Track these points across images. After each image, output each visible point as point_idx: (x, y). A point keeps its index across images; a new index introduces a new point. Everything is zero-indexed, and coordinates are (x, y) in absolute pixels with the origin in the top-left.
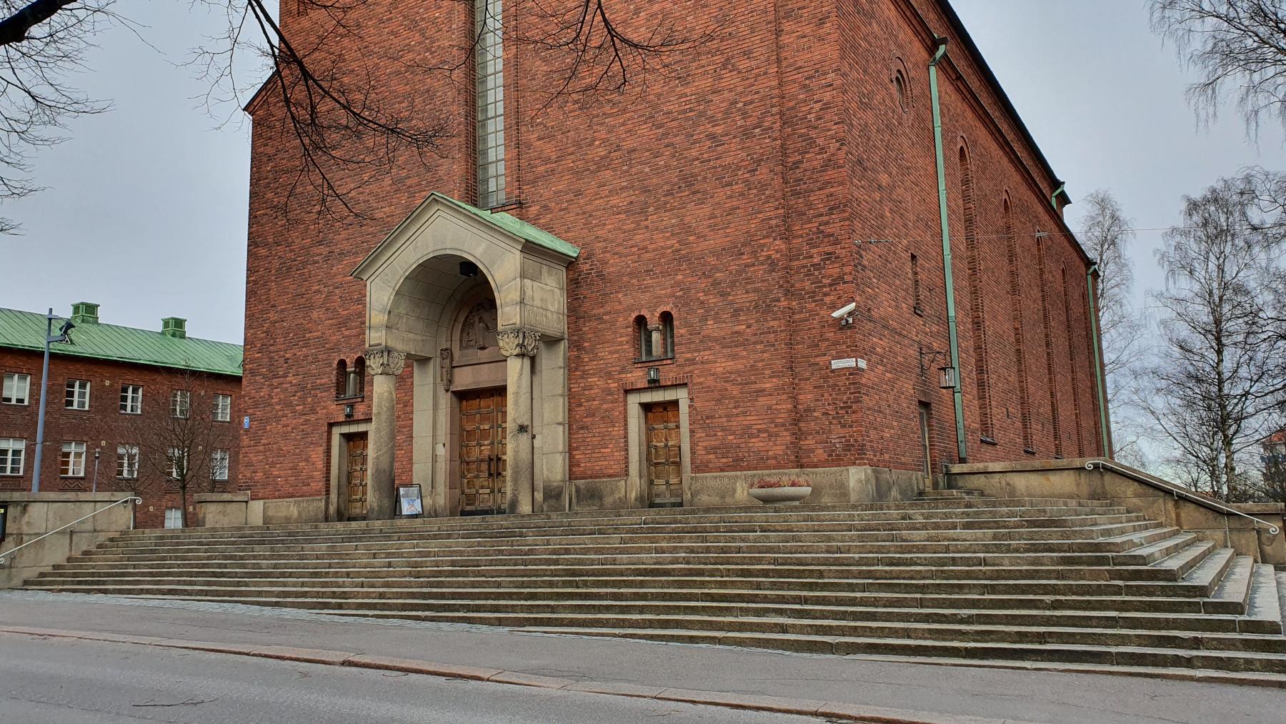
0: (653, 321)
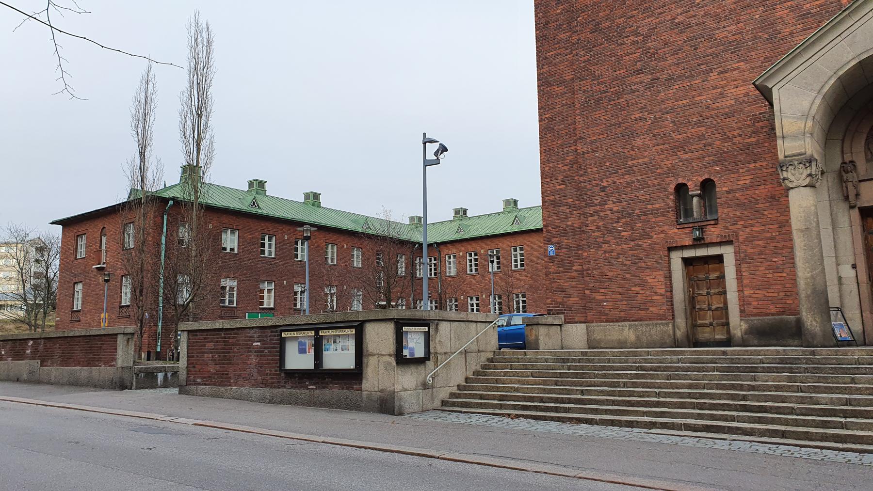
0: (694, 190)
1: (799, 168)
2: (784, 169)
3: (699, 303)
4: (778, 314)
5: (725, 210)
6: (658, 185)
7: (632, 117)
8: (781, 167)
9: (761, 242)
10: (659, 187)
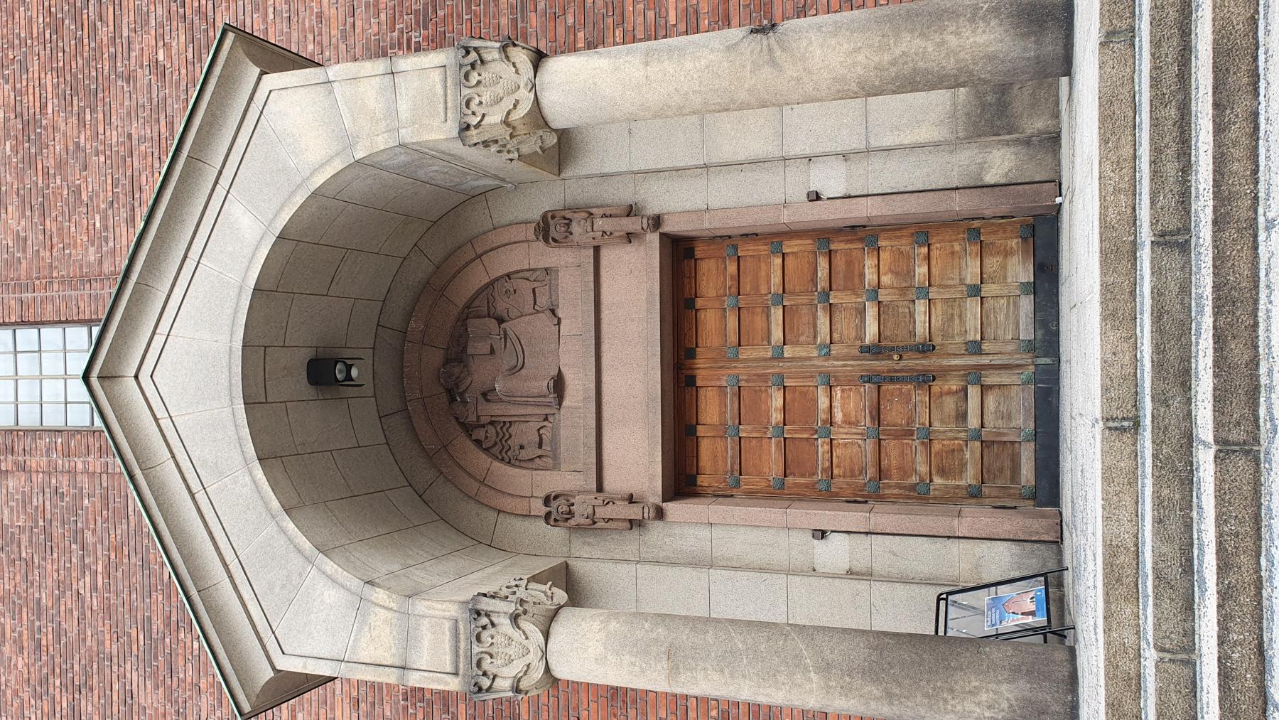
1: (492, 644)
2: (486, 683)
8: (480, 690)
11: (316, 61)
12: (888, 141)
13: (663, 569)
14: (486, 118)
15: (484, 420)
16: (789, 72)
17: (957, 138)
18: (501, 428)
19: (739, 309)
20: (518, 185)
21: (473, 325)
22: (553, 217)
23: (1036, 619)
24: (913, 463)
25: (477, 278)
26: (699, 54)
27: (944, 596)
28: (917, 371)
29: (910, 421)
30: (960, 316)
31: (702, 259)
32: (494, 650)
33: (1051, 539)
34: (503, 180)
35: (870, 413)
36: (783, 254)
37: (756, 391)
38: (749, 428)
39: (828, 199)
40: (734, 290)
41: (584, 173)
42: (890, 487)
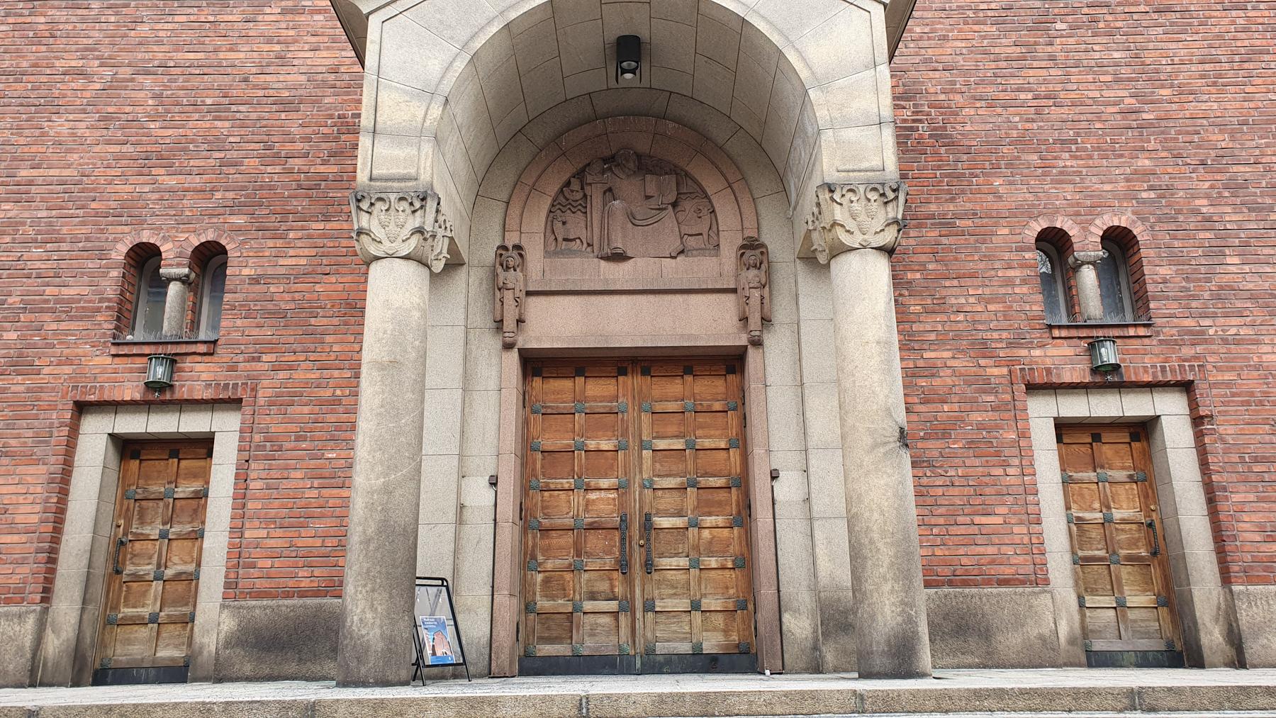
0: (174, 264)
2: (365, 205)
3: (136, 560)
4: (316, 593)
5: (239, 322)
6: (87, 240)
7: (57, 63)
8: (359, 201)
9: (306, 409)
10: (89, 245)
11: (904, 35)
12: (818, 535)
13: (461, 350)
14: (839, 206)
15: (588, 189)
16: (867, 459)
17: (820, 592)
18: (580, 205)
19: (683, 412)
20: (791, 221)
21: (670, 181)
22: (762, 253)
23: (430, 656)
24: (554, 557)
25: (712, 184)
26: (884, 386)
27: (445, 584)
28: (630, 560)
29: (589, 555)
30: (675, 594)
31: (726, 380)
32: (392, 212)
33: (493, 669)
34: (795, 209)
35: (595, 522)
36: (728, 449)
37: (614, 427)
38: (583, 422)
39: (772, 487)
40: (699, 408)
41: (800, 280)
42: (534, 538)
